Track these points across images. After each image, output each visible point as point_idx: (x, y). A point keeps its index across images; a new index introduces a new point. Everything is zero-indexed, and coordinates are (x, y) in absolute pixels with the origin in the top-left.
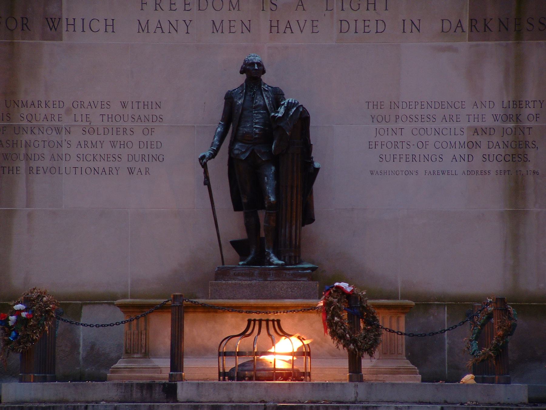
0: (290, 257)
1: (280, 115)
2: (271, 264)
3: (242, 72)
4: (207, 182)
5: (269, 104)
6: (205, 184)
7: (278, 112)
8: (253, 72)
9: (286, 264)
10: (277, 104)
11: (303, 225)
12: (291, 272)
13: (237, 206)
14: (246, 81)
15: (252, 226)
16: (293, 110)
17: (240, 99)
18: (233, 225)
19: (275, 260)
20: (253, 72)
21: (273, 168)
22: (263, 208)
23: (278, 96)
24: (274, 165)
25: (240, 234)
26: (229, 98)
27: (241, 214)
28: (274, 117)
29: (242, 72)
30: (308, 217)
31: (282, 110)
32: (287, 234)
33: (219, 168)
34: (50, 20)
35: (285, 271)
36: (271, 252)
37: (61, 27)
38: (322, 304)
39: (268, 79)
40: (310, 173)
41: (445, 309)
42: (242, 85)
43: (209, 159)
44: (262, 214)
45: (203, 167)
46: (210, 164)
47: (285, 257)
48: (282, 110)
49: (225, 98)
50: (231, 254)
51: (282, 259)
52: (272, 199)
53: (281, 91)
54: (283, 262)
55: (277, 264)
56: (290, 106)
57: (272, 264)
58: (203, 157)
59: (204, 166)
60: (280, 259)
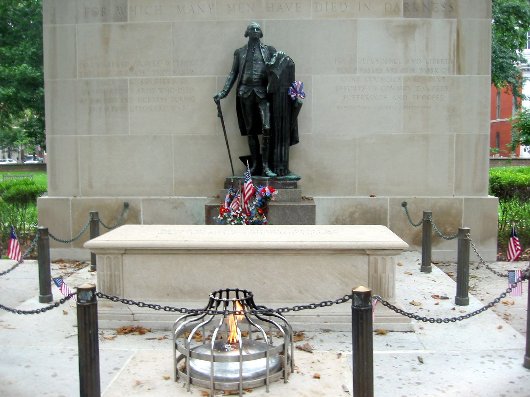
0: (281, 170)
1: (272, 63)
2: (267, 176)
3: (246, 36)
4: (220, 115)
5: (265, 57)
6: (218, 116)
7: (271, 61)
8: (254, 36)
9: (278, 176)
10: (271, 56)
11: (291, 145)
12: (282, 182)
13: (243, 133)
14: (249, 42)
15: (254, 146)
16: (282, 60)
17: (244, 54)
18: (240, 146)
19: (270, 173)
20: (254, 36)
21: (268, 104)
22: (261, 133)
23: (271, 51)
24: (269, 102)
25: (246, 152)
26: (237, 54)
27: (246, 137)
28: (268, 65)
29: (246, 36)
30: (294, 140)
31: (274, 60)
32: (279, 153)
33: (229, 106)
34: (119, 9)
35: (277, 182)
36: (267, 165)
37: (127, 13)
38: (20, 4)
39: (264, 41)
40: (294, 107)
41: (273, 206)
42: (246, 46)
43: (222, 98)
44: (260, 137)
45: (217, 104)
46: (222, 101)
47: (277, 170)
48: (274, 60)
49: (234, 55)
50: (238, 165)
51: (275, 171)
52: (267, 127)
53: (273, 48)
54: (275, 175)
55: (271, 176)
56: (280, 56)
57: (267, 176)
58: (216, 97)
59: (218, 103)
60: (273, 172)
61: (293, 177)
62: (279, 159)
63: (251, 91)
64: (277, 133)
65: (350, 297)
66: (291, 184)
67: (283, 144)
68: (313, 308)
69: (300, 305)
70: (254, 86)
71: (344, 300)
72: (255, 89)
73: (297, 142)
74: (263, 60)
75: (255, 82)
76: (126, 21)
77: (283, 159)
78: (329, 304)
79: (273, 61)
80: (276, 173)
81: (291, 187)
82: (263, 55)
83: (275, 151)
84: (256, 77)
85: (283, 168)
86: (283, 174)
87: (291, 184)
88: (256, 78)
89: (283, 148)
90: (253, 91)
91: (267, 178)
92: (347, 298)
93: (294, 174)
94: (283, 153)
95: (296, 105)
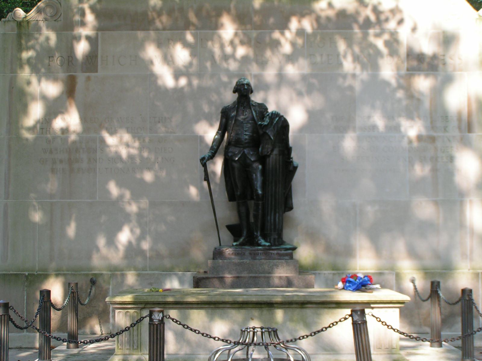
0: (275, 239)
1: (266, 123)
3: (234, 92)
5: (256, 116)
7: (264, 121)
9: (271, 246)
13: (232, 197)
17: (233, 112)
19: (263, 242)
29: (234, 92)
30: (289, 207)
35: (271, 251)
40: (288, 169)
47: (270, 239)
51: (268, 240)
52: (260, 192)
57: (259, 245)
58: (202, 159)
59: (204, 165)
60: (266, 241)
61: (288, 247)
62: (273, 227)
63: (242, 153)
64: (270, 199)
65: (350, 316)
66: (287, 255)
67: (277, 210)
68: (323, 328)
69: (315, 331)
70: (245, 148)
71: (345, 319)
72: (246, 151)
73: (291, 208)
74: (253, 119)
75: (246, 143)
76: (97, 71)
77: (277, 227)
78: (335, 324)
79: (266, 122)
80: (270, 242)
81: (287, 258)
82: (254, 113)
83: (269, 218)
84: (247, 137)
85: (276, 237)
86: (277, 243)
87: (287, 255)
88: (246, 139)
89: (277, 215)
90: (244, 152)
91: (260, 247)
92: (347, 317)
93: (288, 244)
94: (277, 220)
95: (291, 168)
